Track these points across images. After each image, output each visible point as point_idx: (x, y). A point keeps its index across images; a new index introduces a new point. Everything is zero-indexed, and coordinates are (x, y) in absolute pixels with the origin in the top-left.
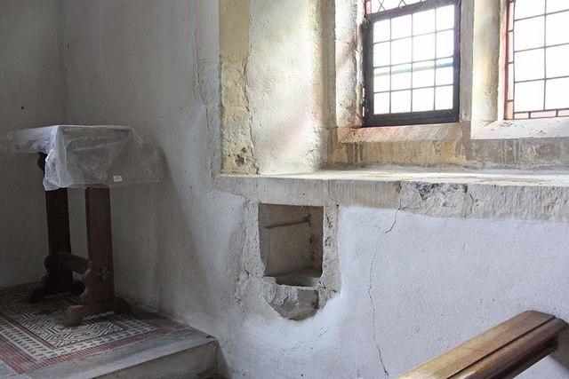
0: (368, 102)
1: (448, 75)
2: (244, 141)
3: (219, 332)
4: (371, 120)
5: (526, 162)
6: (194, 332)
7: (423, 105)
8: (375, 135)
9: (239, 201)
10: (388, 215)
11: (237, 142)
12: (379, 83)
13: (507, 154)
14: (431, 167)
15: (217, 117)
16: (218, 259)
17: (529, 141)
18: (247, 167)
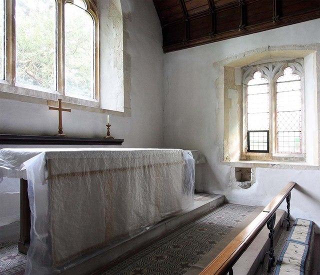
0: (249, 146)
1: (266, 144)
2: (227, 155)
3: (224, 193)
4: (249, 151)
5: (236, 188)
6: (217, 195)
7: (261, 149)
8: (250, 154)
9: (229, 167)
10: (266, 169)
11: (226, 155)
12: (251, 144)
13: (279, 159)
14: (265, 161)
15: (222, 150)
16: (223, 179)
17: (283, 157)
18: (228, 160)
